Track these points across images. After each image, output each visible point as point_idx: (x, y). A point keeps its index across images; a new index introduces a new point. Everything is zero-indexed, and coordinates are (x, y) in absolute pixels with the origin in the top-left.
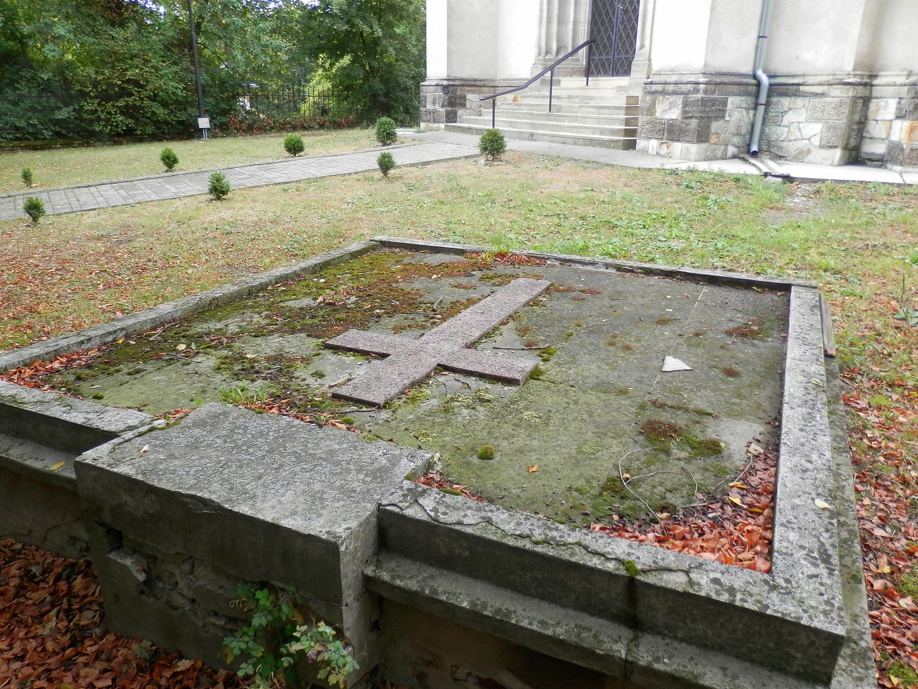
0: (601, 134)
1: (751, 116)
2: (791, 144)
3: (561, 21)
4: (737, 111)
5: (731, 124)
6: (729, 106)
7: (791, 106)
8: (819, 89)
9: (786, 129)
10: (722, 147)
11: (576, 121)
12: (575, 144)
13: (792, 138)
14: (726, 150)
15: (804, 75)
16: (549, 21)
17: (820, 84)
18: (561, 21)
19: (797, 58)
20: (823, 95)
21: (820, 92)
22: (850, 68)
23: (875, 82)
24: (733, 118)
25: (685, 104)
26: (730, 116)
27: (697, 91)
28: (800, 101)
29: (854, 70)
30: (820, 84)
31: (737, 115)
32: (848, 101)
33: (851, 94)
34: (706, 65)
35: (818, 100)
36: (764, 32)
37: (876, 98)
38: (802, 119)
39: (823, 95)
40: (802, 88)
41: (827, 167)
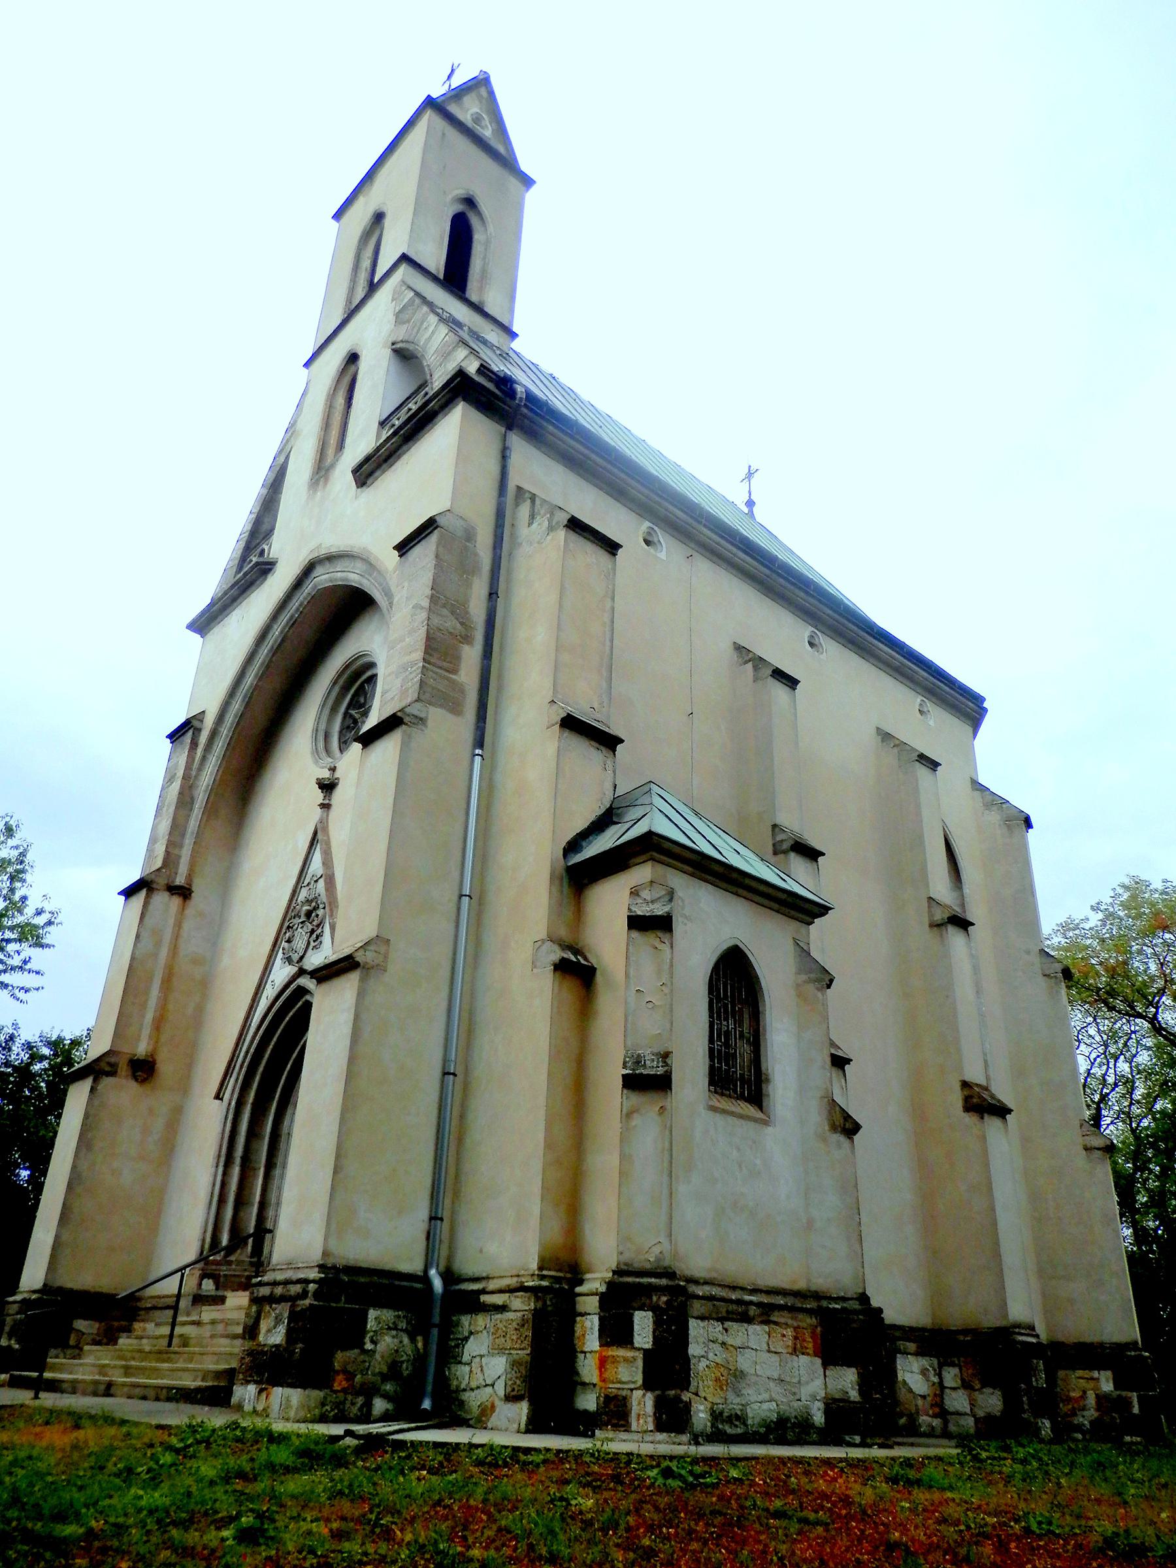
0: (156, 1369)
1: (420, 1345)
2: (473, 1394)
3: (241, 1202)
4: (385, 1336)
5: (378, 1356)
6: (371, 1324)
7: (473, 1329)
8: (498, 1299)
9: (467, 1368)
10: (360, 1400)
11: (191, 1361)
12: (157, 1399)
13: (473, 1384)
14: (368, 1405)
15: (488, 1278)
16: (222, 1200)
17: (501, 1291)
18: (241, 1202)
19: (481, 1251)
20: (503, 1308)
21: (500, 1303)
22: (534, 1266)
23: (578, 1289)
24: (381, 1347)
25: (293, 1316)
26: (373, 1342)
27: (304, 1295)
28: (481, 1320)
29: (540, 1268)
30: (501, 1291)
31: (387, 1342)
32: (530, 1316)
33: (532, 1306)
34: (325, 1254)
35: (499, 1316)
36: (436, 1212)
37: (582, 1315)
38: (484, 1351)
39: (503, 1308)
40: (484, 1298)
41: (507, 1428)
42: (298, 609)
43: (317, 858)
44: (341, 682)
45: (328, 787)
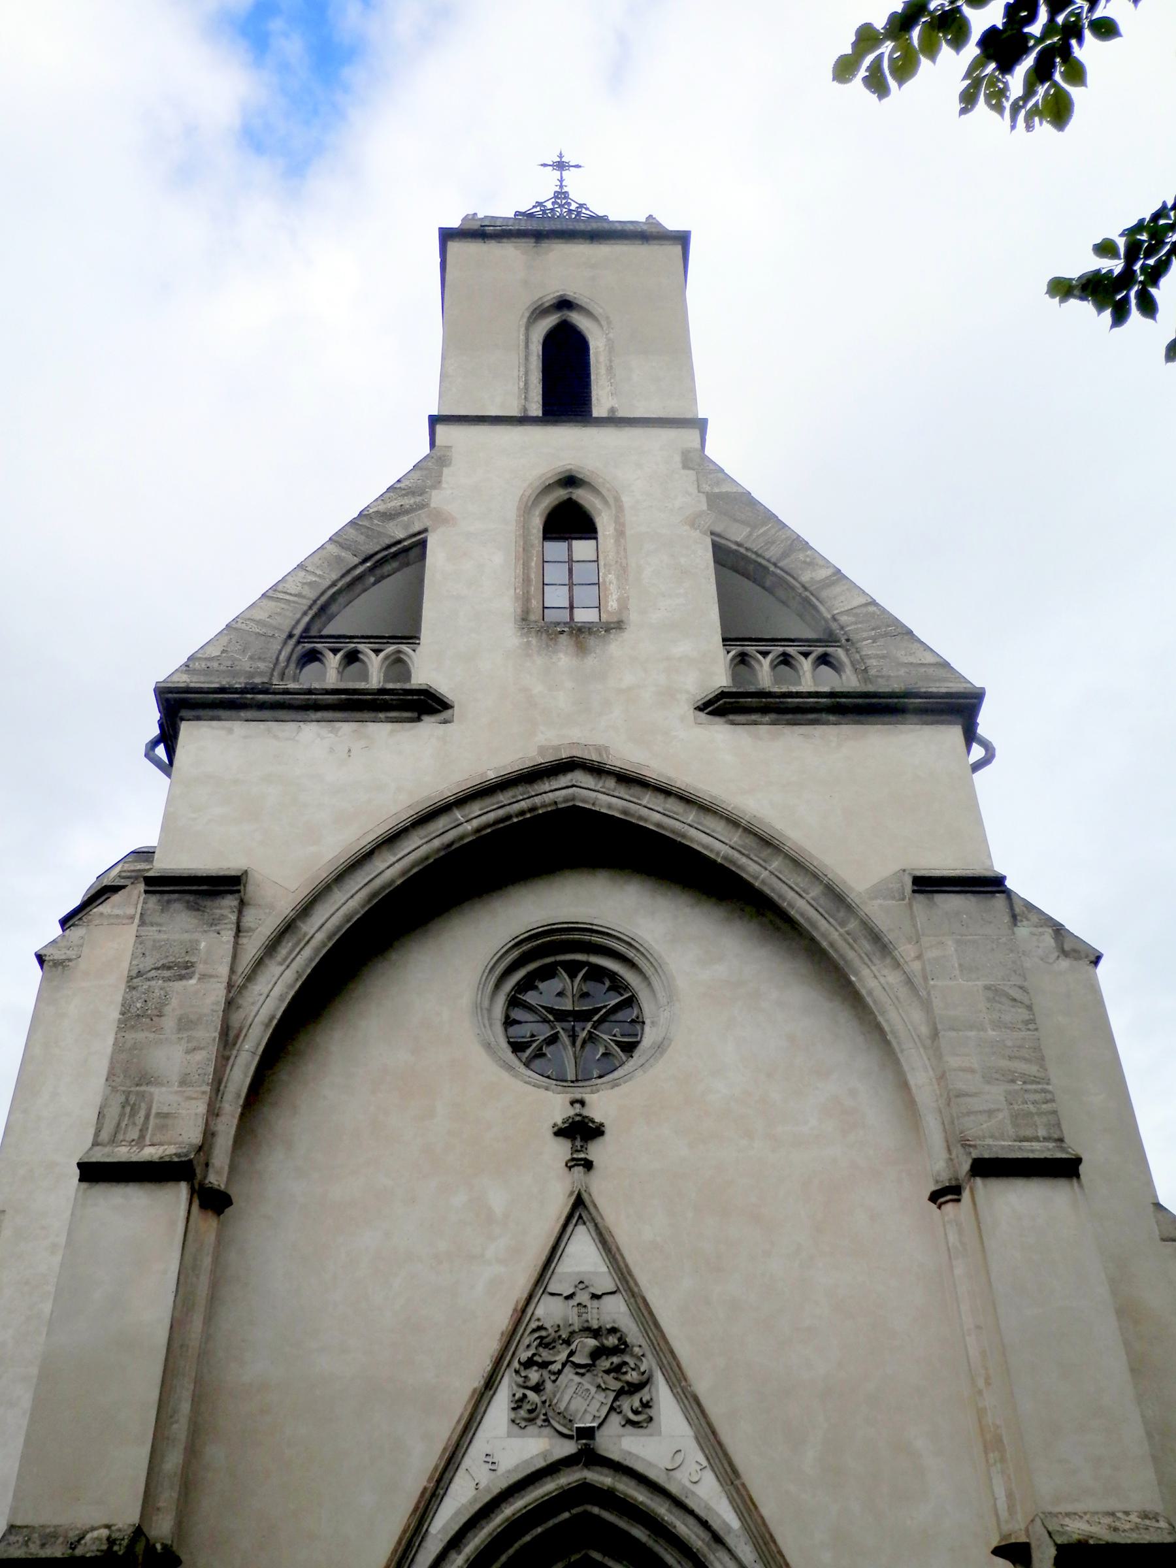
42: (522, 813)
43: (583, 1256)
44: (525, 947)
45: (580, 1131)
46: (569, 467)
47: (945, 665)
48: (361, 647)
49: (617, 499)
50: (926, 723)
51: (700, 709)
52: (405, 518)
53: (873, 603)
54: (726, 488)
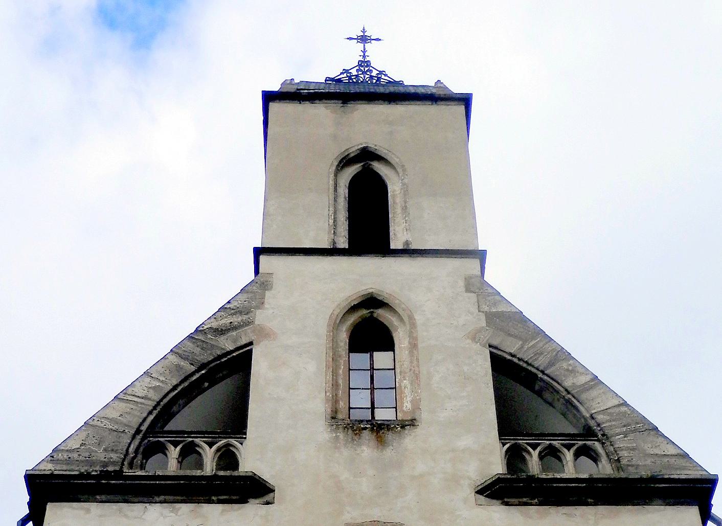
46: (371, 291)
47: (685, 456)
48: (197, 440)
49: (411, 318)
50: (386, 166)
51: (480, 492)
52: (234, 333)
53: (625, 404)
54: (501, 308)
